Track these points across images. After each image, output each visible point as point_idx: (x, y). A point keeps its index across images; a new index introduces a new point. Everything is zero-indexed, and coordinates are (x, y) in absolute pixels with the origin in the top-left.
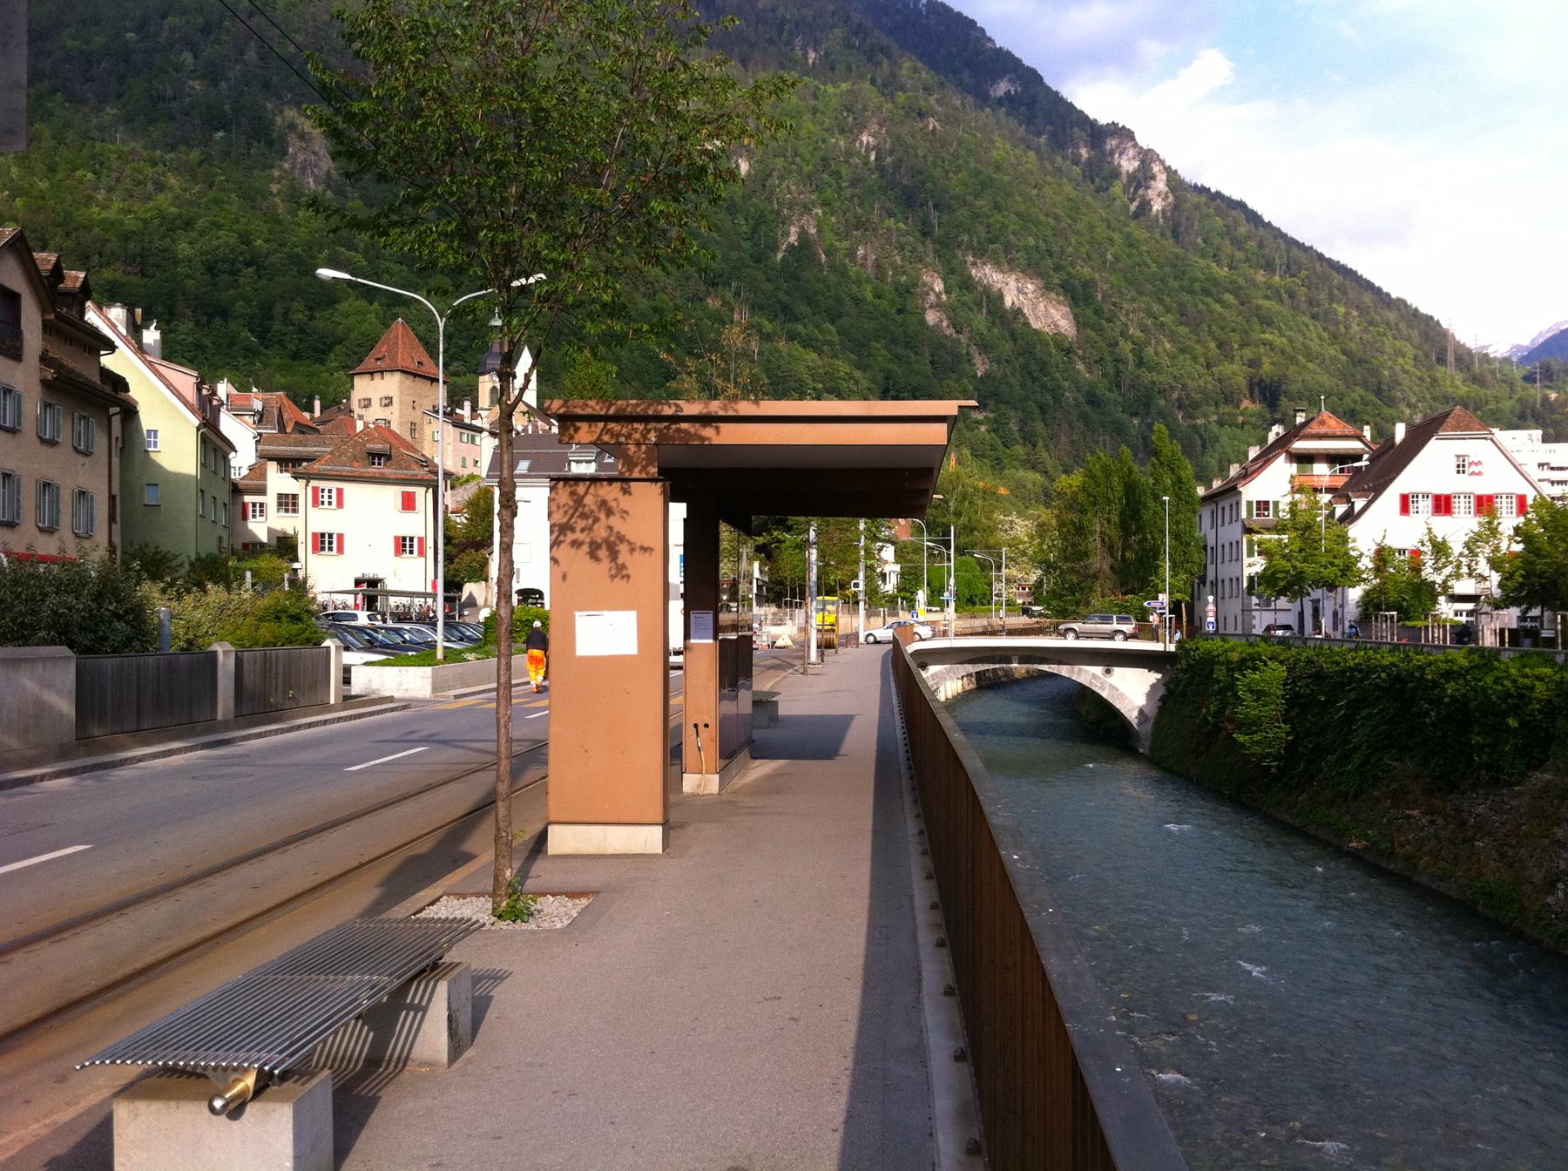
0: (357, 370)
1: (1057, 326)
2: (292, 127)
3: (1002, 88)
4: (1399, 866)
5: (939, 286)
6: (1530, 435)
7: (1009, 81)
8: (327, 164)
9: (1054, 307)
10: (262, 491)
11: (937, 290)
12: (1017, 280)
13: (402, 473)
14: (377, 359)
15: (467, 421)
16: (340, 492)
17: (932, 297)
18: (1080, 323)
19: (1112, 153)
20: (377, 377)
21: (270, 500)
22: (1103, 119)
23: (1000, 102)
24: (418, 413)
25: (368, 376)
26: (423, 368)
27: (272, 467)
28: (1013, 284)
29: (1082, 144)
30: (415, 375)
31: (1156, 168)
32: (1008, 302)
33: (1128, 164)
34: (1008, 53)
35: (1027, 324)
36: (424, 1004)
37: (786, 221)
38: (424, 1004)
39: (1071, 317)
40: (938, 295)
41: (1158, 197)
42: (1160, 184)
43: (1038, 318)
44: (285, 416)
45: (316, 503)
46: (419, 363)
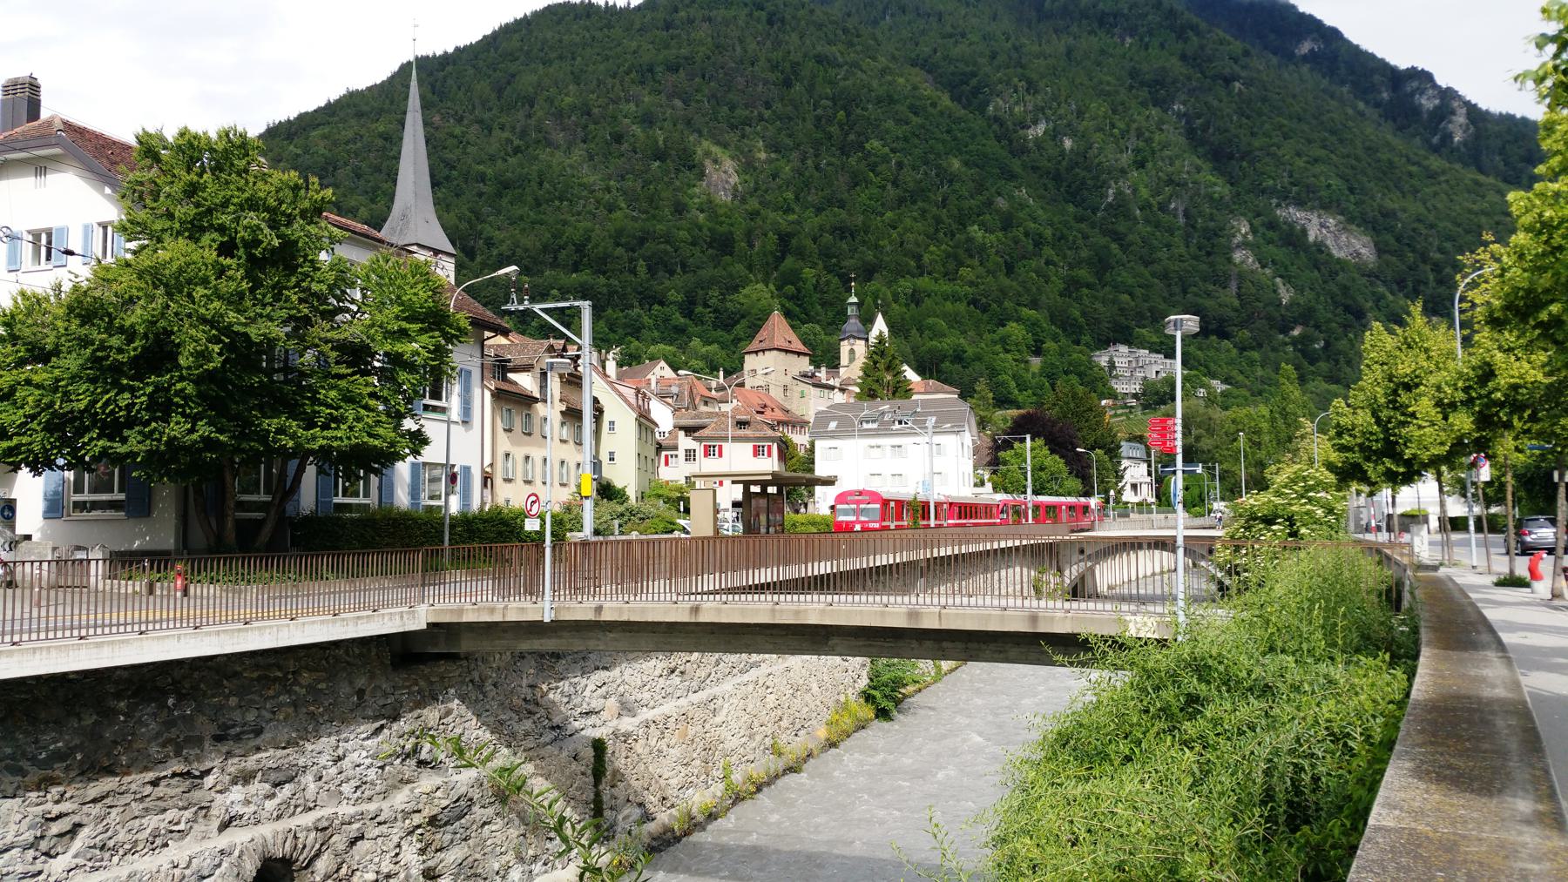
1: (1359, 254)
2: (708, 154)
3: (1305, 47)
7: (1313, 40)
8: (734, 179)
9: (1355, 237)
10: (675, 448)
12: (1319, 216)
13: (758, 434)
15: (824, 381)
16: (720, 447)
17: (1239, 238)
18: (1380, 250)
19: (1412, 94)
20: (761, 354)
21: (681, 453)
22: (1403, 64)
23: (1305, 58)
24: (789, 378)
27: (682, 433)
28: (1315, 220)
29: (1383, 89)
30: (787, 351)
31: (1455, 104)
32: (1311, 238)
33: (1428, 103)
34: (1311, 16)
35: (1330, 255)
37: (1105, 185)
39: (1372, 245)
41: (1458, 130)
42: (1461, 118)
43: (1340, 248)
44: (695, 391)
45: (707, 454)
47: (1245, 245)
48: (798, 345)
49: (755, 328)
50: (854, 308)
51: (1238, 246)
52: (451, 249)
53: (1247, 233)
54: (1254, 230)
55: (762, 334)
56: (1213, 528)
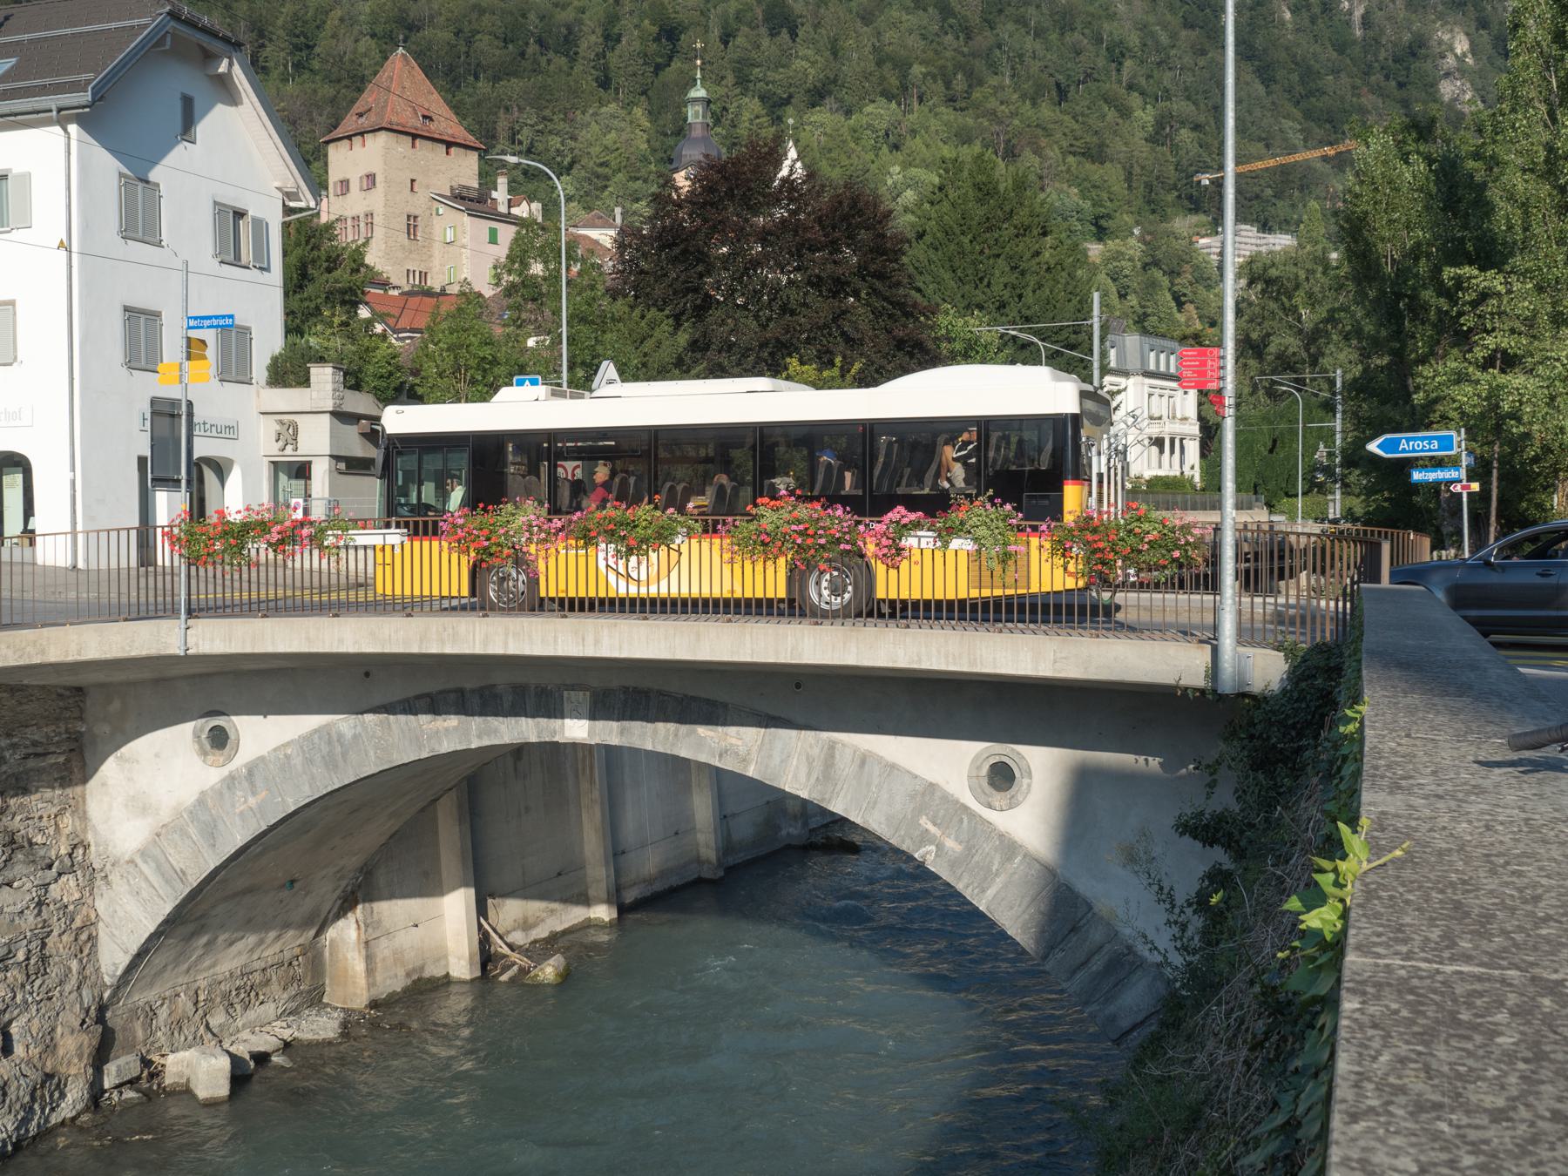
0: (334, 135)
4: (789, 556)
5: (1461, 45)
6: (832, 746)
11: (1459, 51)
14: (360, 115)
17: (1450, 61)
20: (357, 140)
25: (346, 142)
26: (433, 126)
36: (193, 569)
38: (193, 569)
40: (1460, 59)
46: (425, 117)
47: (1462, 71)
48: (447, 123)
49: (359, 83)
50: (699, 108)
51: (1447, 75)
52: (471, 139)
53: (1464, 55)
54: (1474, 50)
55: (368, 98)
56: (1392, 564)
